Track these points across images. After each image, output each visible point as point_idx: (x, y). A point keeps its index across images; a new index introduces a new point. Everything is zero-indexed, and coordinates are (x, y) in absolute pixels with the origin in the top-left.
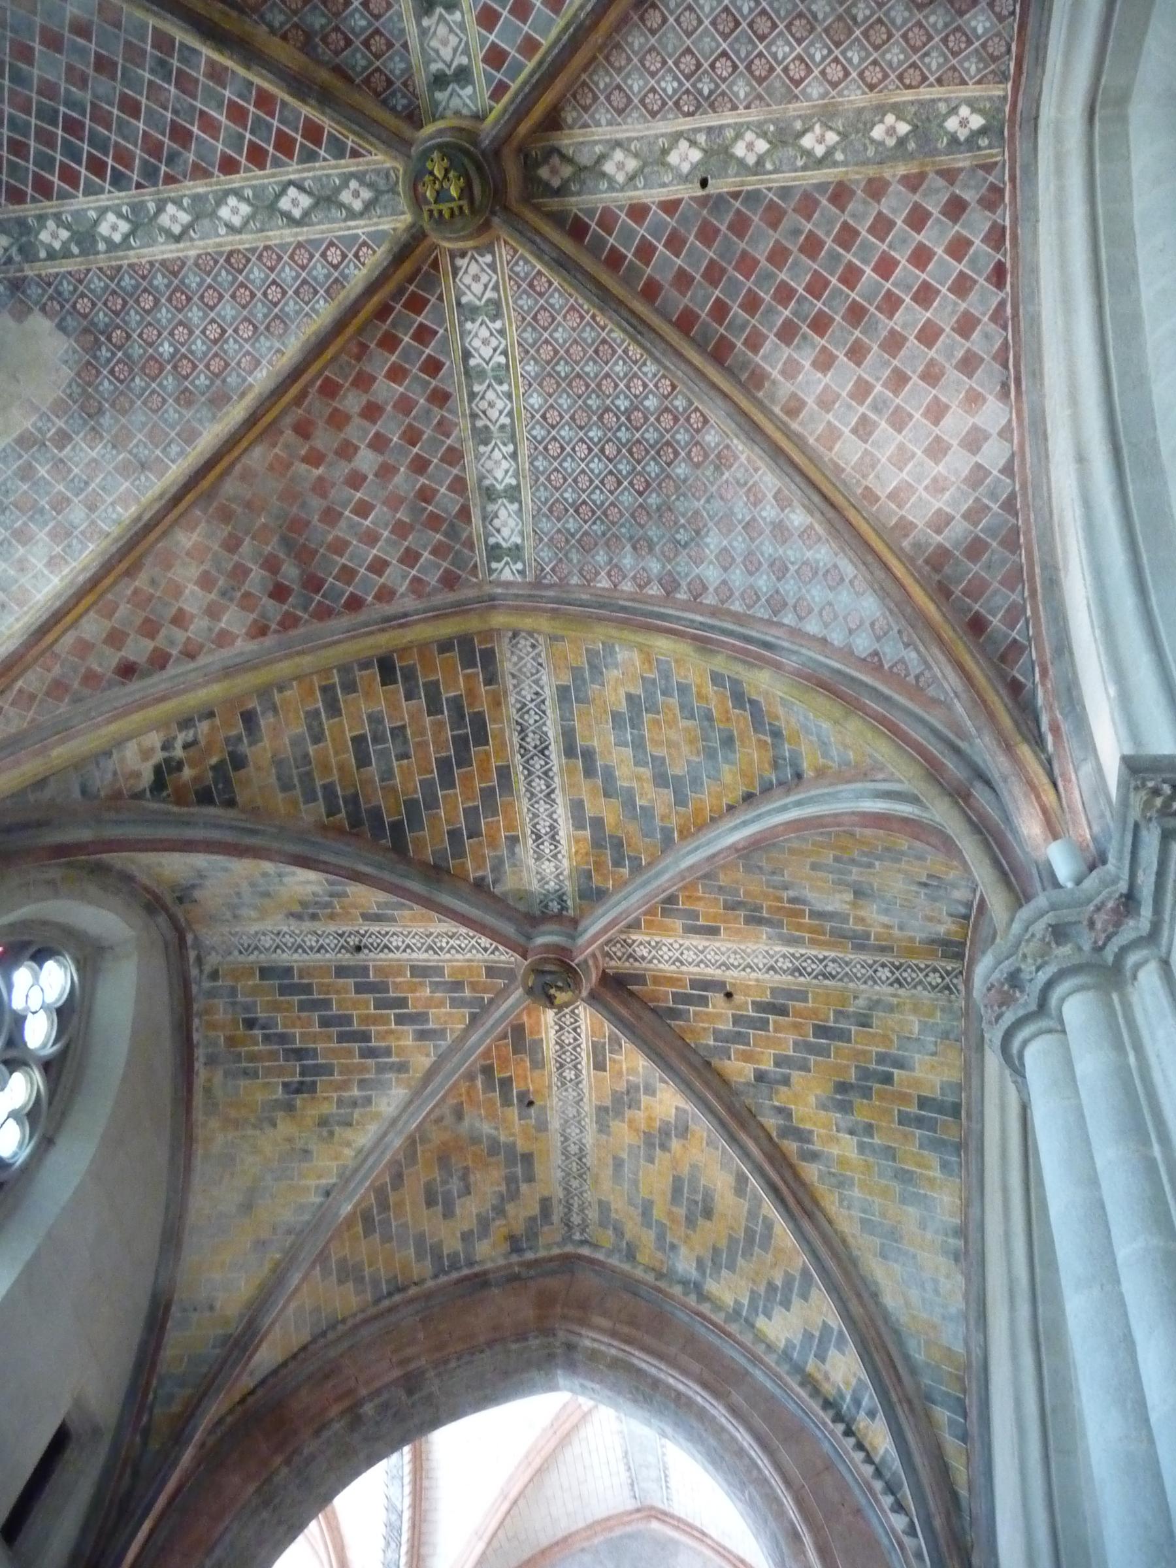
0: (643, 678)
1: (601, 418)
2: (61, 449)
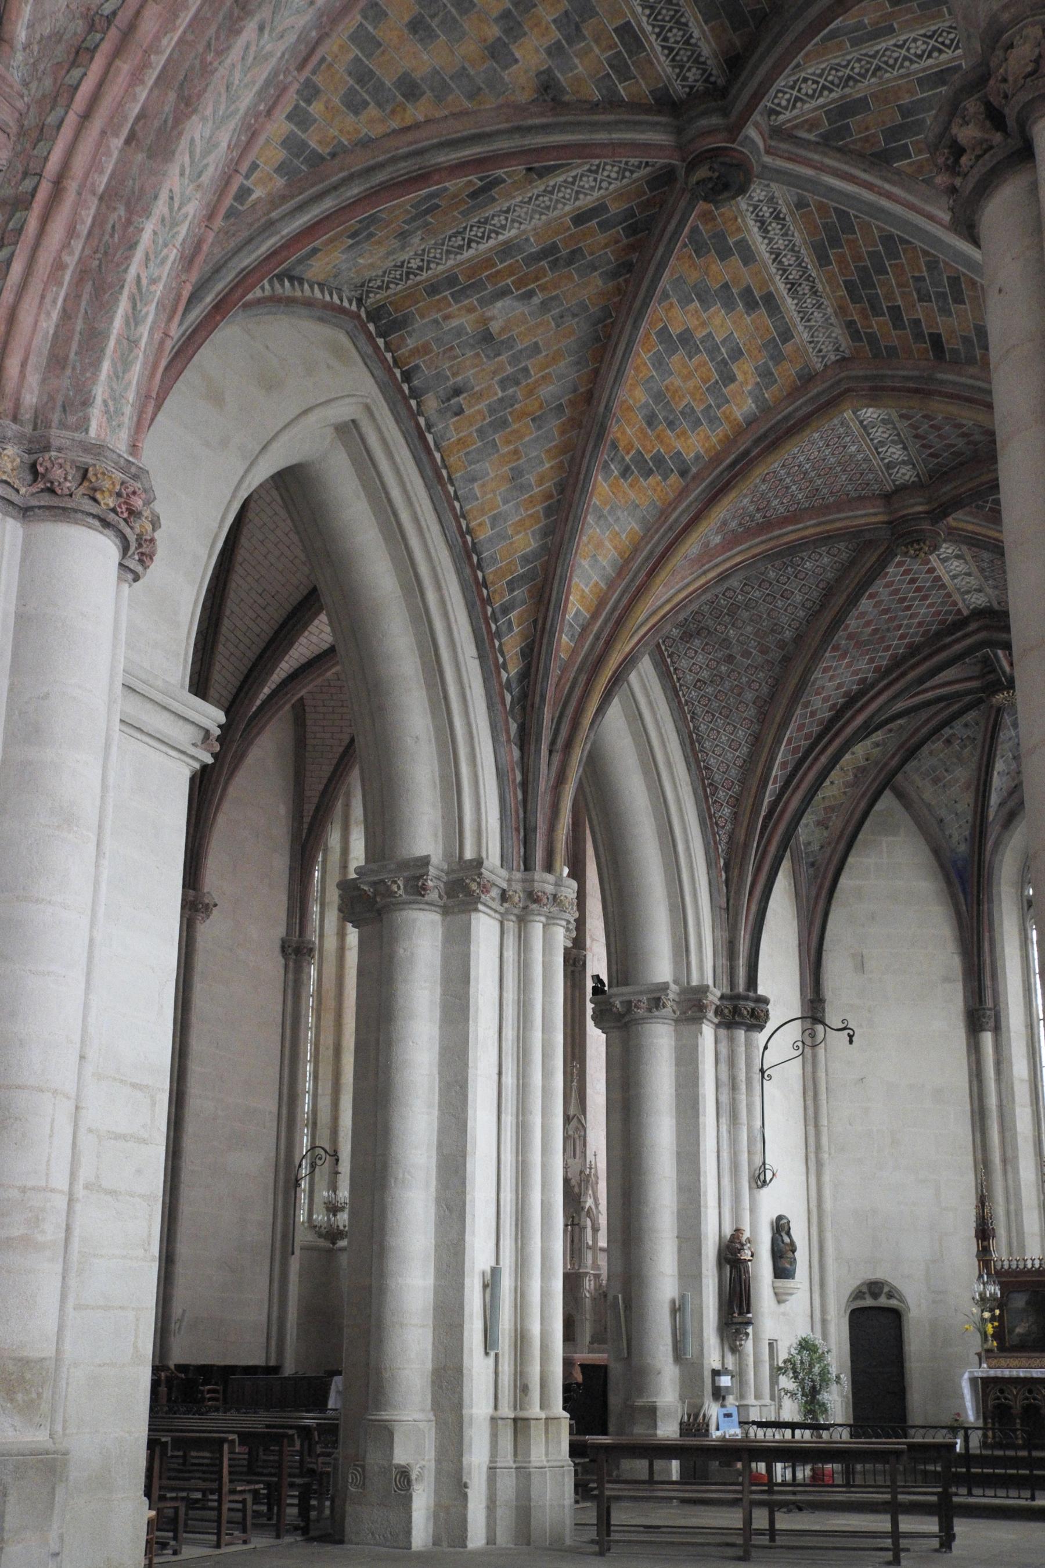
0: (728, 402)
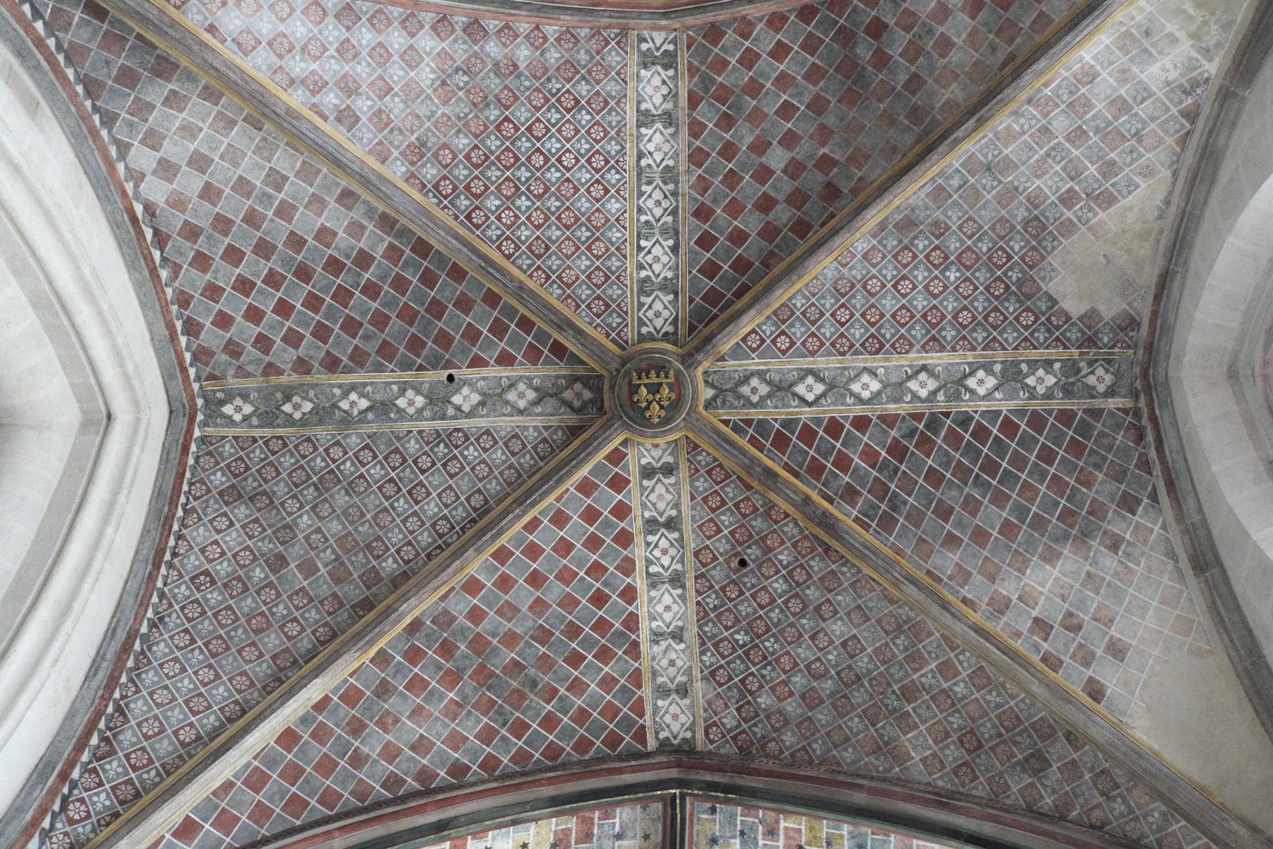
1: (547, 189)
2: (1070, 190)
